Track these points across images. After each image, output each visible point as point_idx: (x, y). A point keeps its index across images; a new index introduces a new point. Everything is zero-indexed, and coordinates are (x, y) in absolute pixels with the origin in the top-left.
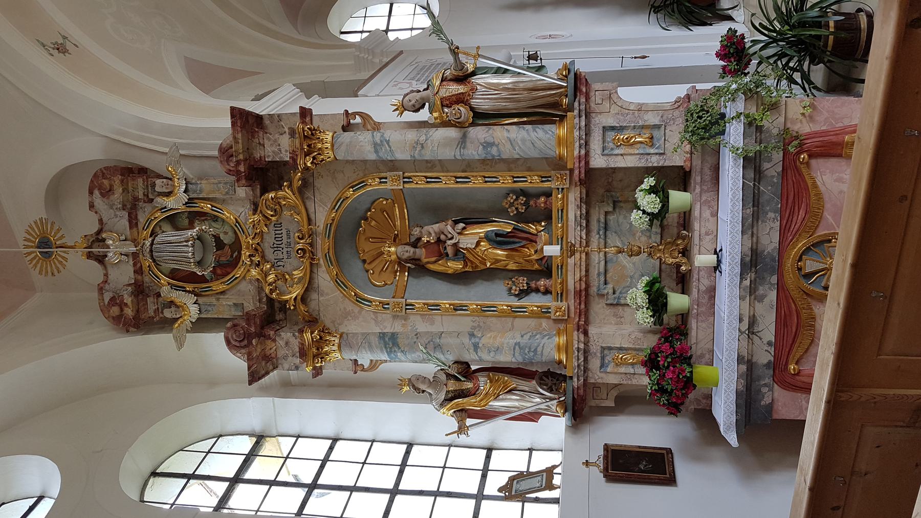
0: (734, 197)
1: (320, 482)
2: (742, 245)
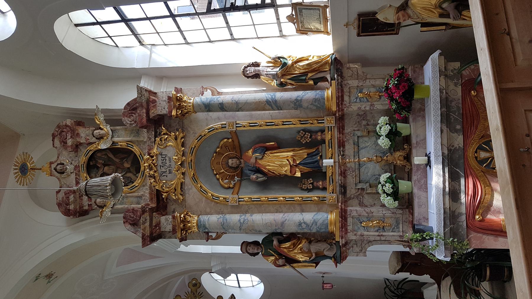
0: (436, 142)
1: (168, 14)
2: (441, 145)
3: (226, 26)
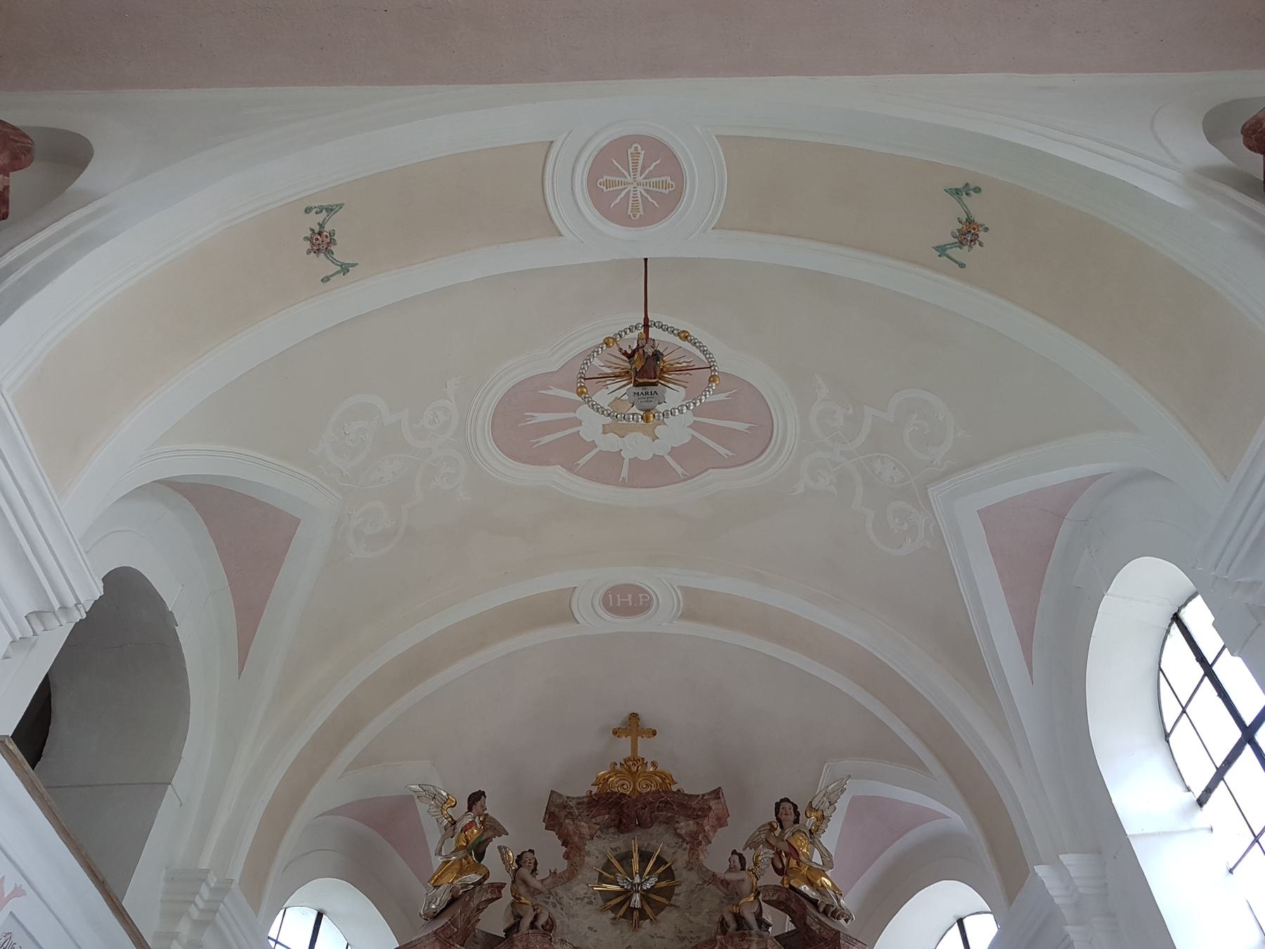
1: (1248, 721)
3: (1218, 767)
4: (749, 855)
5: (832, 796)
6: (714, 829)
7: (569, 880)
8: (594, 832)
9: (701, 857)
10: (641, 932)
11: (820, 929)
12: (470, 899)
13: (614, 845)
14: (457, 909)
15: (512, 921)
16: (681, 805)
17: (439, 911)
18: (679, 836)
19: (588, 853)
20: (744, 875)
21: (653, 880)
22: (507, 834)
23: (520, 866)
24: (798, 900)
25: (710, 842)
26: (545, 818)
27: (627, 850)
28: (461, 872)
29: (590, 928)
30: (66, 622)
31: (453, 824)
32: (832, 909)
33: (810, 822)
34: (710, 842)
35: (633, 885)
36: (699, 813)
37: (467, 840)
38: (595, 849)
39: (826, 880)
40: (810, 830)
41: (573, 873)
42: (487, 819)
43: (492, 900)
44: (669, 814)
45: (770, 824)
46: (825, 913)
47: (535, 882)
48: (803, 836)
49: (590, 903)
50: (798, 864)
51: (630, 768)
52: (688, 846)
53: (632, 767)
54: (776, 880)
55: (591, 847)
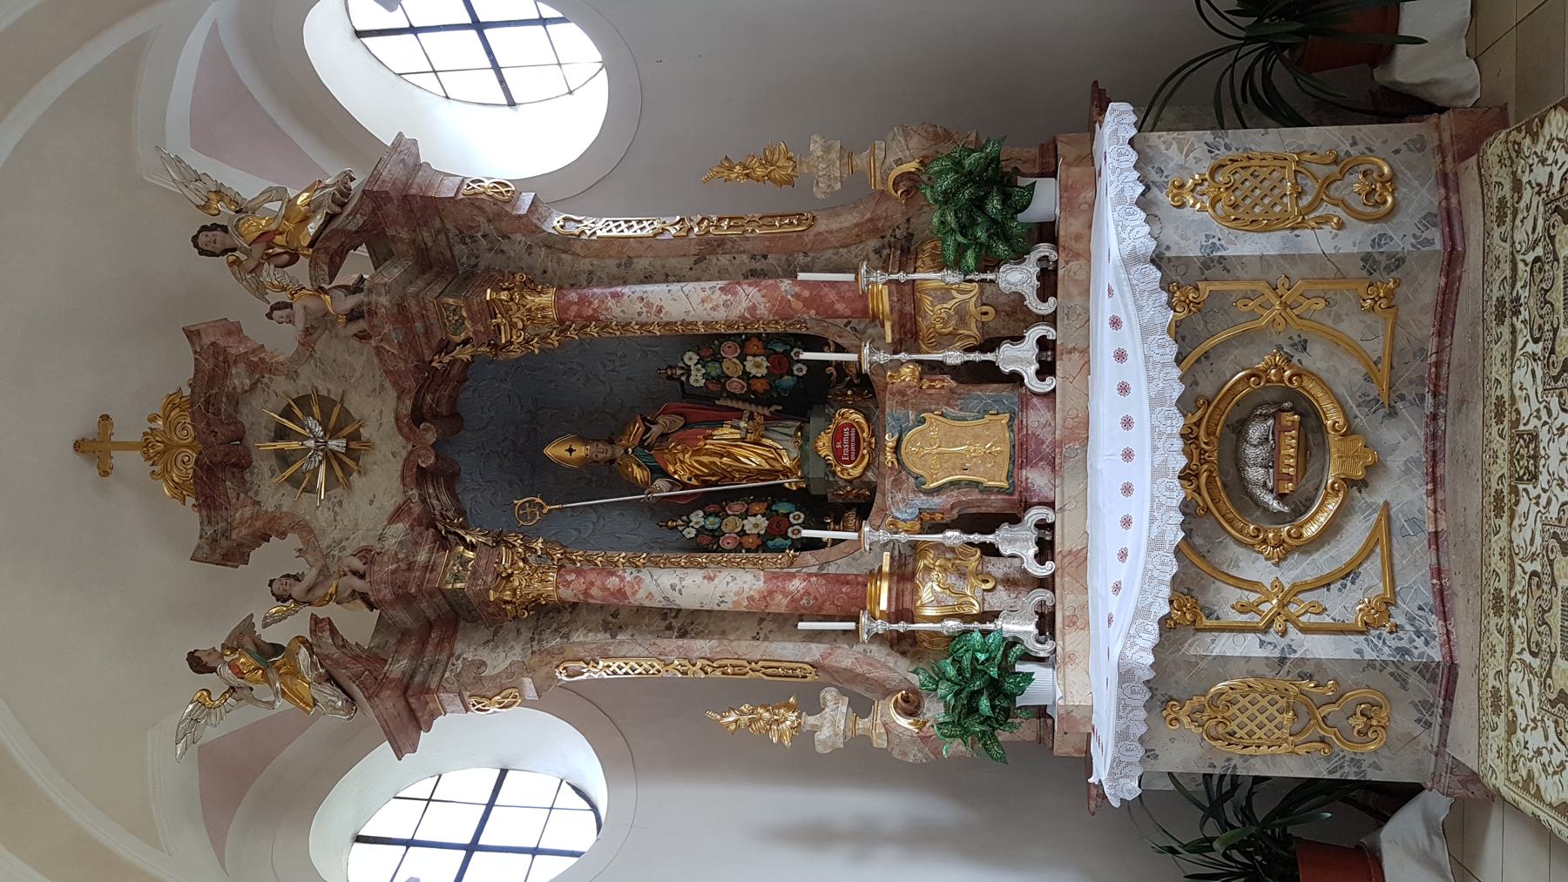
4: (275, 297)
5: (187, 176)
6: (243, 339)
7: (311, 531)
8: (250, 501)
9: (281, 359)
10: (375, 439)
11: (361, 214)
12: (331, 659)
13: (267, 474)
14: (342, 674)
15: (359, 601)
16: (210, 386)
17: (345, 696)
18: (253, 386)
19: (278, 507)
20: (297, 306)
21: (311, 422)
22: (252, 615)
23: (290, 597)
24: (327, 238)
25: (262, 346)
26: (232, 566)
27: (274, 456)
28: (295, 673)
29: (371, 503)
30: (974, 634)
31: (234, 691)
32: (338, 195)
33: (226, 212)
34: (262, 346)
35: (317, 449)
36: (221, 358)
37: (254, 670)
38: (273, 497)
39: (301, 199)
40: (237, 212)
41: (303, 526)
42: (230, 645)
43: (334, 632)
44: (224, 400)
45: (231, 264)
46: (343, 205)
47: (311, 576)
48: (244, 223)
49: (340, 503)
50: (280, 234)
51: (159, 453)
52: (267, 375)
53: (156, 449)
54: (303, 262)
55: (269, 505)
